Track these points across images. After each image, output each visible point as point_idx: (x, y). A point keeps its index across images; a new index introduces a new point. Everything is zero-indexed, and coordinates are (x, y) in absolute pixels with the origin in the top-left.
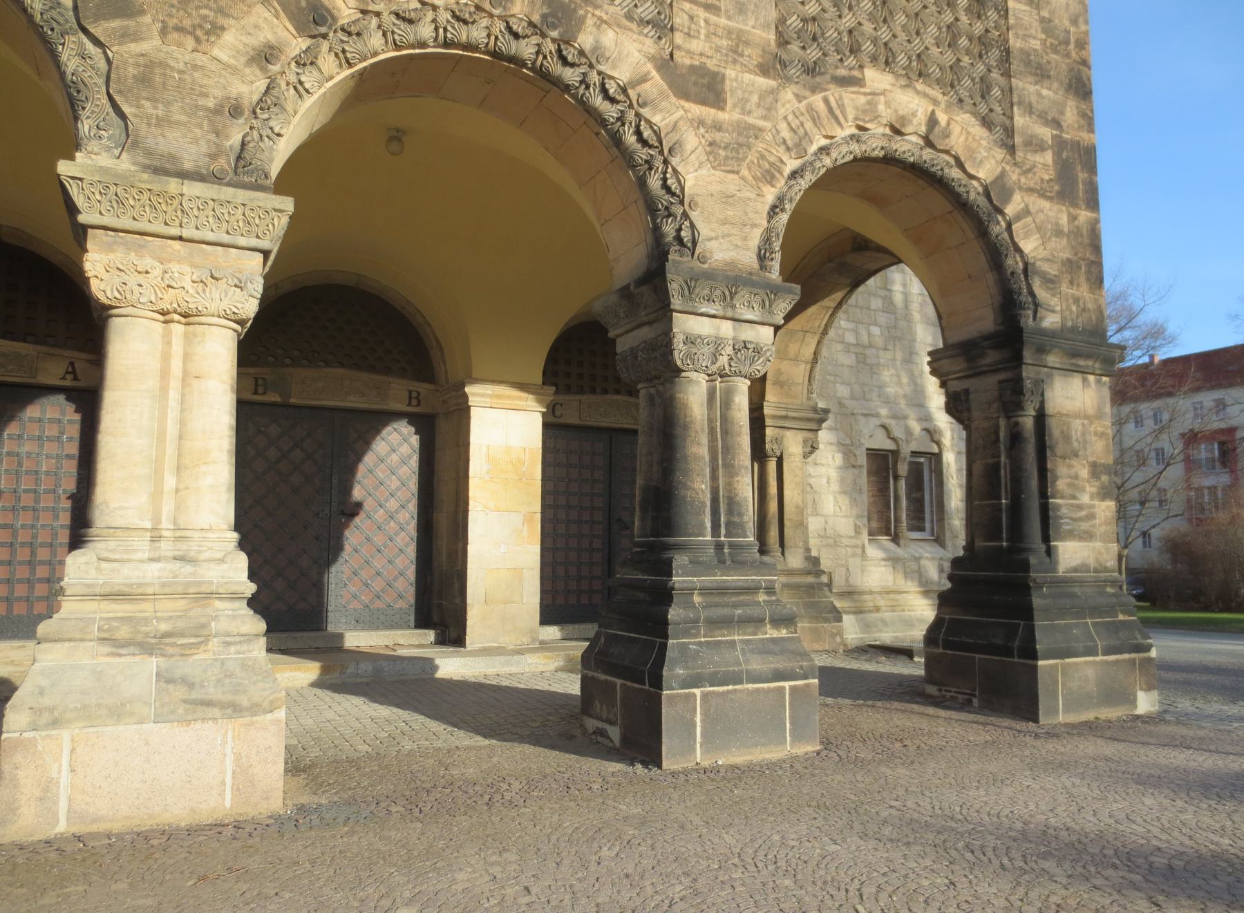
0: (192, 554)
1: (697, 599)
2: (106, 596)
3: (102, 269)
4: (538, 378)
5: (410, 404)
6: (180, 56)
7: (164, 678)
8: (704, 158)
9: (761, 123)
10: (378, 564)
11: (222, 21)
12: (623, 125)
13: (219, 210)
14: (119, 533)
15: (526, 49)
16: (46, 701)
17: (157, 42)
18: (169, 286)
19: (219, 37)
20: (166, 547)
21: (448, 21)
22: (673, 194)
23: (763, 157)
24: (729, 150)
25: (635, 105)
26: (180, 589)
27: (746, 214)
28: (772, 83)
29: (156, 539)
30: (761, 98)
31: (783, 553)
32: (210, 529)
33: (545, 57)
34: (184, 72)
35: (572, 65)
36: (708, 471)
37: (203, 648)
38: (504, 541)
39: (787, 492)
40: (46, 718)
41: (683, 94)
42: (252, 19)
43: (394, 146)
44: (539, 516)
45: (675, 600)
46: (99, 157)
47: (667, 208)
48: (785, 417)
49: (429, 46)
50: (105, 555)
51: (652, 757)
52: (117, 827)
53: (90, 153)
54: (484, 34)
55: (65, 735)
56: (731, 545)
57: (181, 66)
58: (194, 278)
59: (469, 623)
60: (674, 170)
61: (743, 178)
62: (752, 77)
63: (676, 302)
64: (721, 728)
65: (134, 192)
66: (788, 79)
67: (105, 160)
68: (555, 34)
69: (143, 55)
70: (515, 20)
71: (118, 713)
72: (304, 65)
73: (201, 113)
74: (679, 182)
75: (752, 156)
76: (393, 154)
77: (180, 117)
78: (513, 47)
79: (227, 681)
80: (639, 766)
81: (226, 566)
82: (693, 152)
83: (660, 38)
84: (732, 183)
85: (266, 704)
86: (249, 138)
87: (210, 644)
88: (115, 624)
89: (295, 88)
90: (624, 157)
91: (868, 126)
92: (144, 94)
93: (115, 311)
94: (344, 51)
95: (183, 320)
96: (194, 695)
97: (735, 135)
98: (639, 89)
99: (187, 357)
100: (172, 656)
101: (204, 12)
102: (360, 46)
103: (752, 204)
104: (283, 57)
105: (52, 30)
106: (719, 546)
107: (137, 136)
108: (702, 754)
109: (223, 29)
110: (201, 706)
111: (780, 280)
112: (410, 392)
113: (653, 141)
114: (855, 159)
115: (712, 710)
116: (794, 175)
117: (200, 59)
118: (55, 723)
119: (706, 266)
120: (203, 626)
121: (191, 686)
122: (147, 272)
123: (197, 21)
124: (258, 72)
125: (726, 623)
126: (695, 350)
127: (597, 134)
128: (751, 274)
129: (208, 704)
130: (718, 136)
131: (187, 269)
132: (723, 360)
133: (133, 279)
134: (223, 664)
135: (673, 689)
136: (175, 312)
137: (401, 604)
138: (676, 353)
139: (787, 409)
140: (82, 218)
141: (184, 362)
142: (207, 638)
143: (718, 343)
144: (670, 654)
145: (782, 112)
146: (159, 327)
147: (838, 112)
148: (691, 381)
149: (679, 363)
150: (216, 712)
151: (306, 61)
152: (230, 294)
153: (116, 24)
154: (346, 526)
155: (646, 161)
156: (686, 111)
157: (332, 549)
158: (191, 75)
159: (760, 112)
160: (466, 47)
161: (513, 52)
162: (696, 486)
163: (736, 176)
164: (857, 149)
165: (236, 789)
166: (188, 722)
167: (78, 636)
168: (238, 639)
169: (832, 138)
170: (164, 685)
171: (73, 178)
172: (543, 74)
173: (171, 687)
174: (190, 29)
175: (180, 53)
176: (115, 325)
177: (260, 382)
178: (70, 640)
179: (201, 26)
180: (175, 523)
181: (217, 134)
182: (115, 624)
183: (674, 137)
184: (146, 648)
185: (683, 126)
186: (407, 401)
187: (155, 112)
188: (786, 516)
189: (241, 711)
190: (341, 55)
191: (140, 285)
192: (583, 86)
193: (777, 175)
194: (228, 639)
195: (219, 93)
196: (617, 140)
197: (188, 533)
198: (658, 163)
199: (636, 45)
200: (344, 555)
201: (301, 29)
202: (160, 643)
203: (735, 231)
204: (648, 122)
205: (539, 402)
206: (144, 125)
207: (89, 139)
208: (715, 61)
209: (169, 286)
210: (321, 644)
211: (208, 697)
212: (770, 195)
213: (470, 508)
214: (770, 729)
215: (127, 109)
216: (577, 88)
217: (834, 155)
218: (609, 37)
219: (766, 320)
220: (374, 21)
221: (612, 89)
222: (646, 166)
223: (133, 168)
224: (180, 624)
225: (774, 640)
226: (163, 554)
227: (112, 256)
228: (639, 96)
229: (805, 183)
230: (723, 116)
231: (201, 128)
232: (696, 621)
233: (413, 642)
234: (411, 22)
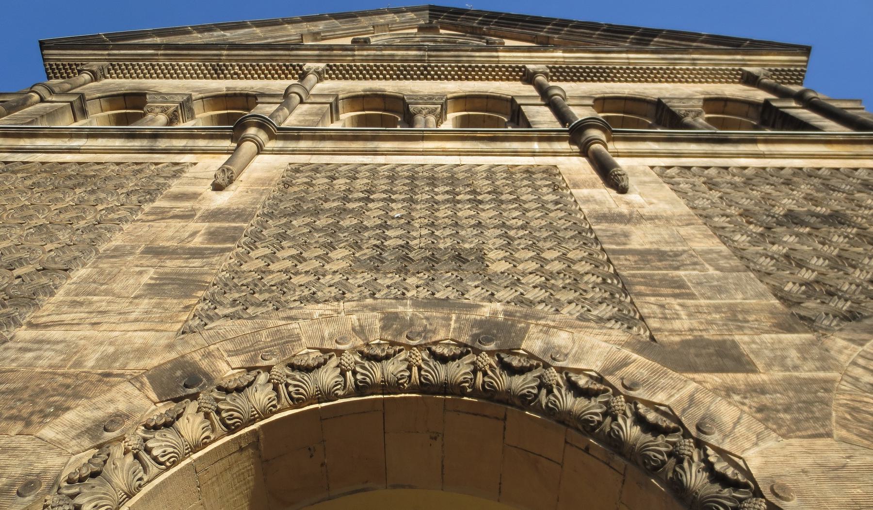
8: (760, 427)
12: (615, 419)
15: (459, 371)
21: (356, 363)
25: (621, 389)
33: (485, 374)
49: (338, 397)
60: (722, 453)
61: (843, 440)
62: (774, 336)
68: (492, 346)
74: (736, 466)
78: (442, 373)
83: (629, 328)
89: (136, 456)
90: (635, 463)
94: (218, 412)
109: (68, 409)
113: (665, 423)
127: (587, 450)
130: (766, 400)
155: (670, 455)
163: (829, 441)
172: (489, 394)
186: (99, 109)
196: (615, 444)
198: (687, 447)
199: (599, 337)
204: (649, 404)
216: (536, 396)
228: (622, 379)
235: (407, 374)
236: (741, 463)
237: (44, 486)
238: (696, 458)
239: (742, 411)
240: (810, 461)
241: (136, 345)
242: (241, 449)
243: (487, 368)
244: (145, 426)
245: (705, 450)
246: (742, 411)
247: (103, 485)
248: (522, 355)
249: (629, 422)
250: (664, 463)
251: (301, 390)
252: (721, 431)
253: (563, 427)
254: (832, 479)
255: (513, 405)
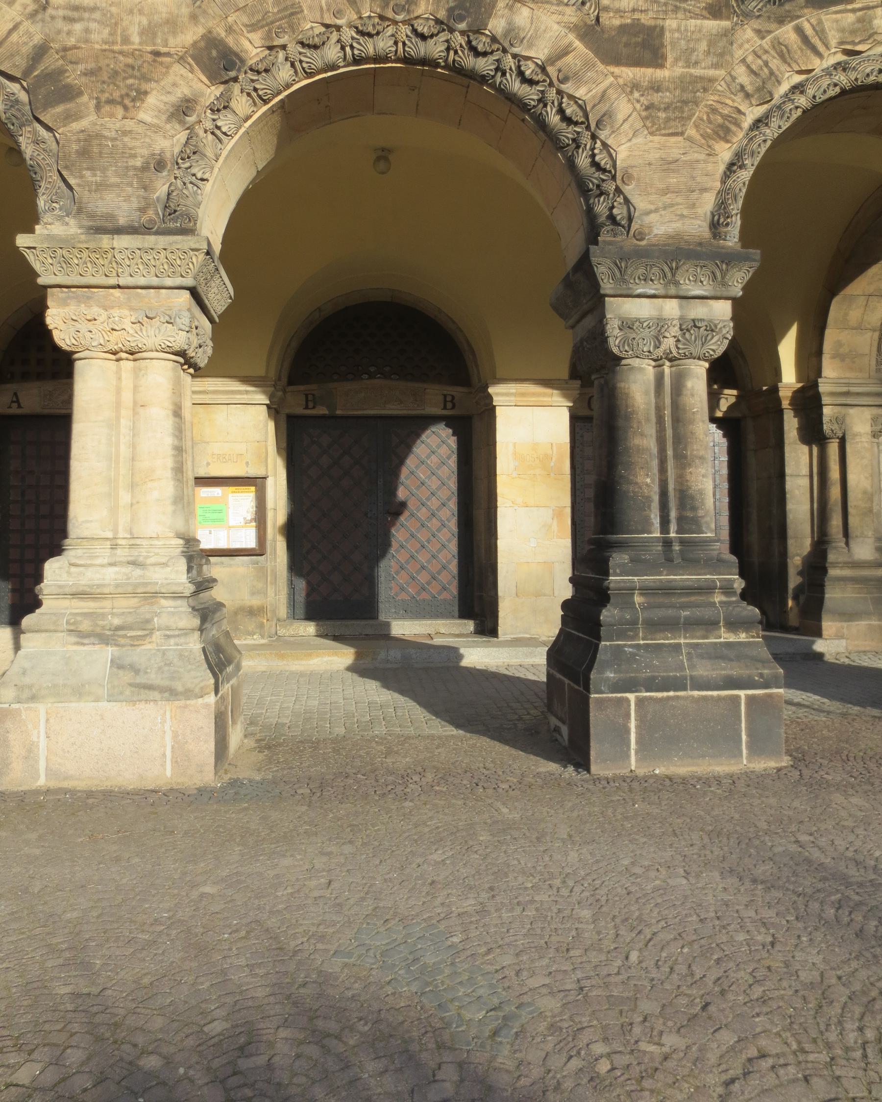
0: (141, 559)
1: (638, 599)
2: (75, 595)
3: (62, 322)
4: (564, 373)
5: (445, 408)
6: (112, 126)
7: (117, 665)
8: (639, 124)
9: (711, 73)
10: (422, 558)
11: (145, 86)
12: (545, 105)
13: (146, 257)
14: (85, 542)
15: (435, 48)
16: (27, 680)
17: (93, 117)
18: (113, 329)
19: (143, 101)
20: (122, 554)
21: (353, 38)
22: (604, 171)
23: (714, 111)
24: (667, 113)
26: (130, 589)
27: (693, 178)
28: (726, 24)
29: (114, 547)
30: (711, 43)
31: (847, 544)
32: (157, 538)
33: (456, 52)
34: (116, 139)
35: (485, 54)
36: (655, 463)
37: (148, 640)
38: (533, 537)
39: (851, 478)
40: (26, 694)
41: (612, 58)
42: (170, 79)
43: (382, 165)
44: (568, 511)
45: (612, 601)
46: (53, 226)
47: (598, 186)
48: (847, 394)
49: (339, 67)
50: (74, 561)
51: (582, 762)
52: (81, 785)
53: (46, 224)
54: (391, 42)
55: (41, 708)
56: (682, 542)
57: (113, 134)
58: (133, 320)
59: (501, 614)
60: (605, 145)
62: (699, 22)
63: (607, 286)
64: (659, 735)
65: (76, 251)
66: (748, 15)
67: (57, 229)
68: (462, 26)
69: (82, 131)
70: (420, 21)
71: (79, 692)
72: (218, 110)
73: (131, 173)
74: (610, 155)
75: (700, 112)
76: (383, 173)
77: (114, 180)
78: (421, 49)
79: (166, 668)
80: (571, 769)
81: (169, 569)
82: (624, 121)
84: (675, 147)
85: (197, 690)
86: (172, 188)
87: (154, 636)
88: (79, 618)
89: (213, 133)
91: (859, 48)
92: (85, 165)
93: (76, 356)
94: (256, 90)
95: (130, 357)
96: (138, 680)
97: (677, 93)
98: (559, 64)
99: (136, 388)
100: (123, 646)
101: (130, 81)
102: (270, 81)
103: (700, 166)
104: (198, 108)
105: (13, 125)
106: (667, 543)
107: (80, 203)
108: (636, 761)
109: (146, 93)
110: (144, 689)
111: (738, 247)
112: (445, 396)
114: (843, 92)
115: (649, 717)
116: (758, 123)
117: (129, 124)
118: (33, 698)
119: (644, 243)
120: (148, 621)
121: (137, 672)
122: (95, 320)
123: (123, 92)
124: (177, 126)
125: (671, 625)
126: (634, 335)
128: (700, 244)
129: (149, 687)
130: (656, 98)
131: (126, 312)
132: (669, 343)
133: (83, 327)
134: (164, 654)
135: (602, 692)
136: (122, 351)
137: (445, 595)
138: (611, 341)
139: (848, 384)
140: (41, 281)
141: (134, 394)
142: (150, 634)
143: (660, 325)
144: (600, 656)
145: (739, 54)
146: (112, 365)
147: (816, 41)
148: (632, 368)
149: (615, 350)
150: (156, 695)
151: (222, 106)
152: (163, 331)
153: (60, 109)
154: (393, 523)
155: (574, 140)
156: (616, 77)
157: (380, 545)
158: (122, 140)
159: (710, 60)
160: (377, 59)
161: (422, 53)
162: (639, 479)
163: (680, 138)
164: (843, 79)
165: (175, 762)
166: (134, 702)
167: (52, 628)
168: (177, 633)
169: (809, 71)
170: (115, 670)
171: (29, 248)
173: (121, 672)
174: (119, 100)
175: (112, 123)
176: (78, 365)
177: (310, 398)
178: (46, 631)
179: (127, 95)
180: (131, 533)
181: (145, 188)
182: (79, 618)
183: (603, 108)
184: (104, 639)
185: (612, 94)
186: (442, 406)
187: (94, 179)
188: (851, 502)
189: (176, 695)
190: (254, 94)
191: (90, 332)
192: (499, 74)
193: (733, 128)
194: (168, 633)
195: (145, 152)
196: (541, 124)
197: (138, 542)
198: (586, 139)
199: (554, 17)
200: (392, 551)
201: (214, 78)
202: (112, 636)
203: (679, 200)
204: (571, 97)
205: (566, 396)
206: (86, 193)
207: (45, 212)
208: (651, 14)
209: (113, 329)
210: (369, 631)
211: (150, 682)
212: (725, 153)
213: (499, 504)
214: (723, 739)
215: (72, 181)
216: (493, 77)
217: (810, 92)
218: (523, 16)
219: (719, 294)
220: (281, 55)
221: (529, 69)
222: (574, 145)
223: (79, 231)
224: (130, 619)
225: (729, 645)
226: (118, 559)
227: (67, 310)
228: (560, 71)
229: (771, 132)
230: (661, 74)
231: (132, 186)
232: (634, 622)
233: (447, 631)
234: (315, 47)
235: (394, 49)
236: (614, 155)
237: (169, 165)
238: (588, 147)
239: (635, 109)
240: (657, 156)
241: (164, 15)
242: (273, 112)
243: (458, 48)
244: (211, 109)
245: (595, 143)
246: (635, 109)
247: (202, 159)
248: (487, 36)
249: (554, 110)
250: (568, 145)
251: (313, 67)
252: (612, 127)
253: (509, 103)
254: (664, 170)
255: (475, 79)
